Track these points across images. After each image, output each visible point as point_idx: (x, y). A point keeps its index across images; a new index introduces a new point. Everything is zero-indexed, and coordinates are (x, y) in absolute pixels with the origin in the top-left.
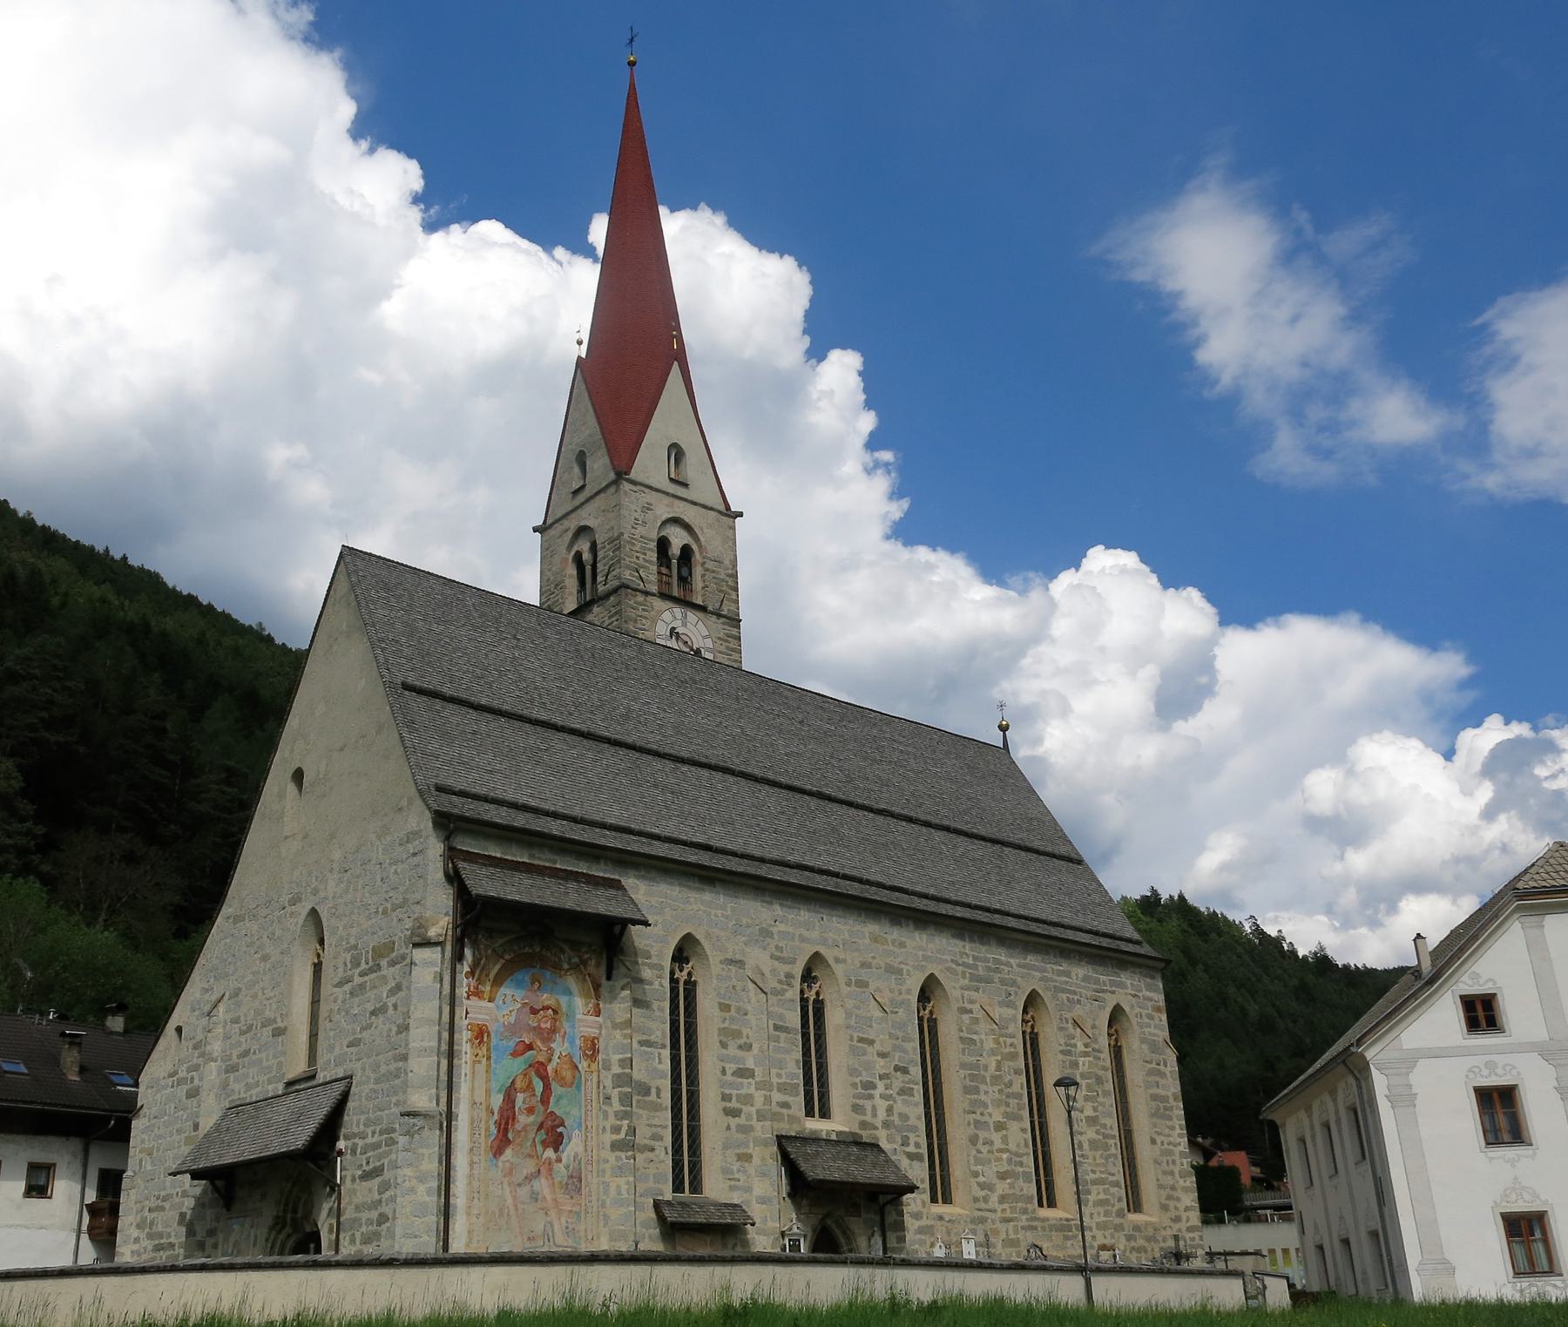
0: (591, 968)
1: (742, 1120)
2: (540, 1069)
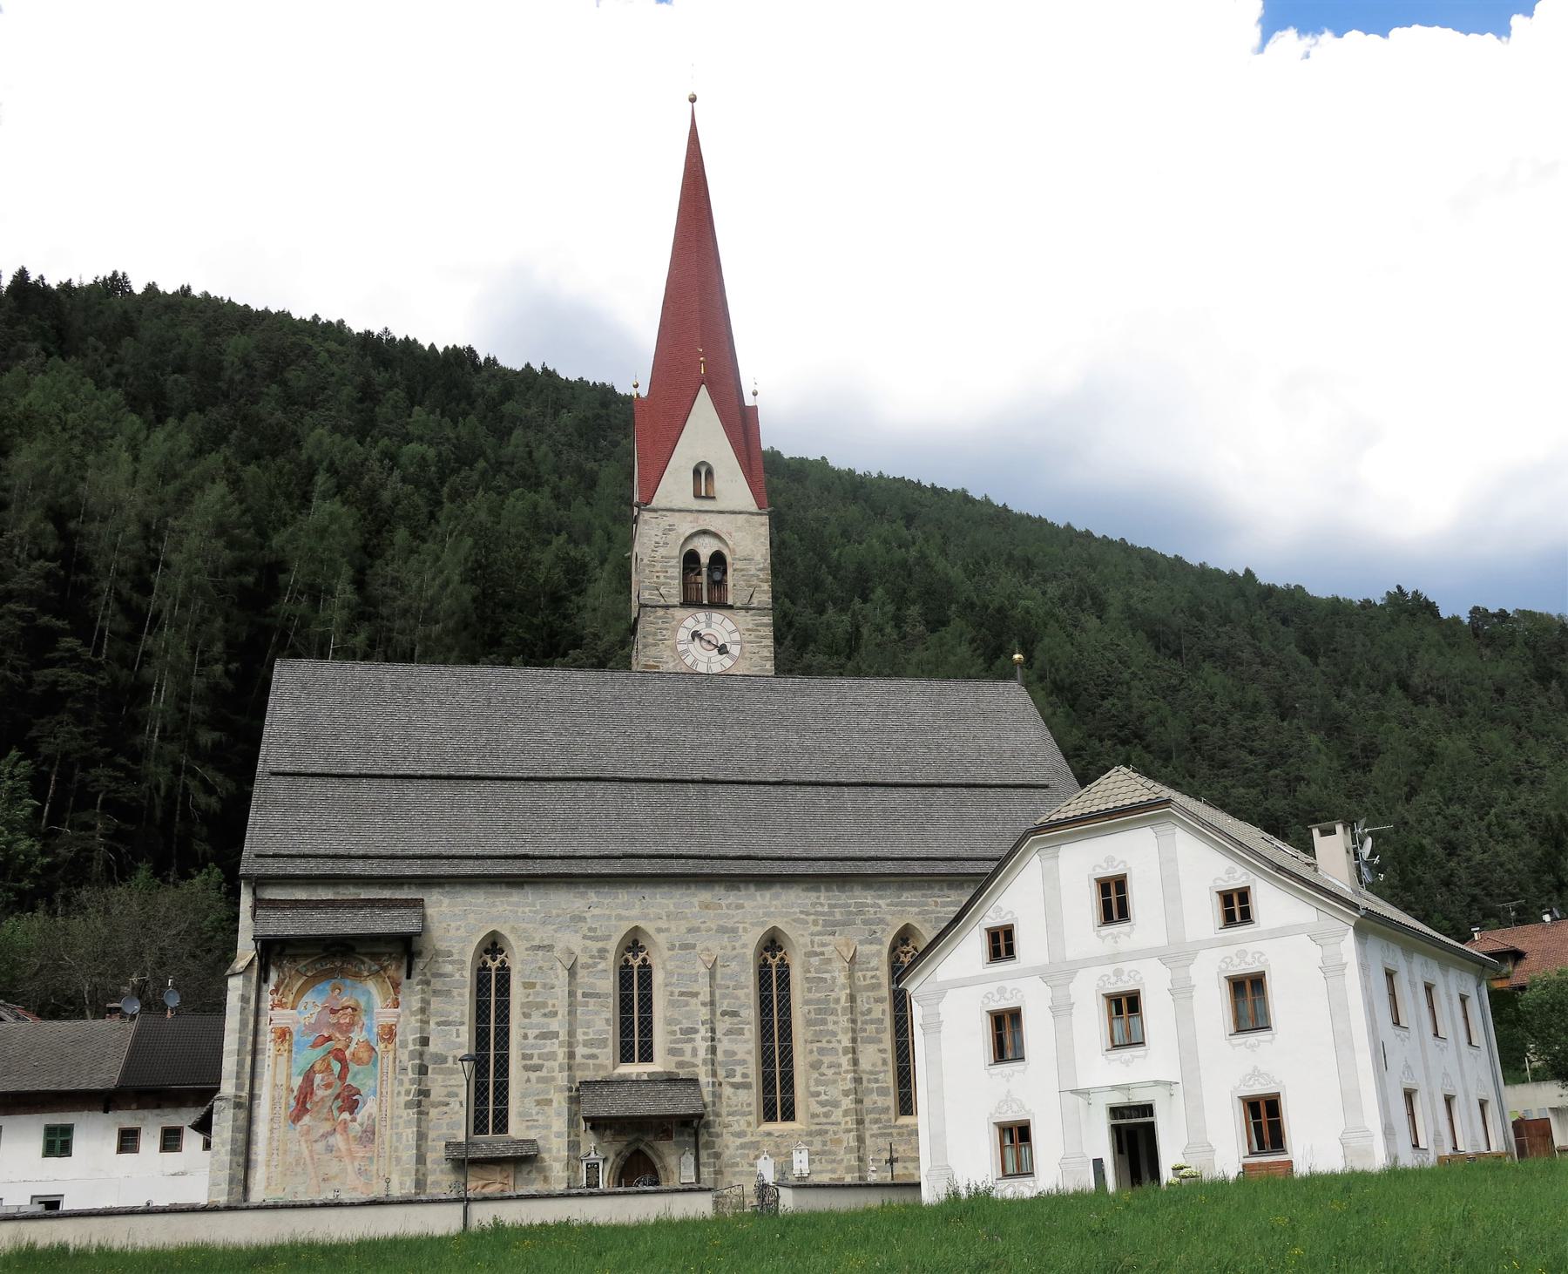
0: (392, 971)
1: (544, 1073)
2: (339, 1055)
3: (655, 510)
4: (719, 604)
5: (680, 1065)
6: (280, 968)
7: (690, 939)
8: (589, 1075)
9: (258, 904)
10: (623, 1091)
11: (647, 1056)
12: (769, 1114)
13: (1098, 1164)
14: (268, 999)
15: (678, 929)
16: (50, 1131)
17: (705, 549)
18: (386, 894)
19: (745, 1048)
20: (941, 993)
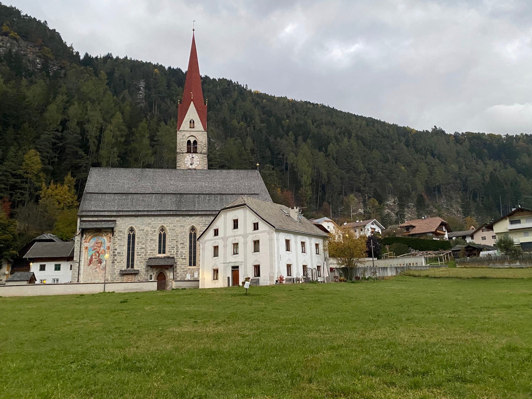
0: (109, 235)
1: (141, 256)
2: (98, 252)
4: (195, 152)
5: (171, 254)
6: (86, 234)
7: (174, 228)
9: (81, 221)
10: (417, 236)
11: (164, 253)
12: (190, 265)
13: (229, 278)
14: (83, 241)
15: (171, 226)
16: (56, 265)
17: (192, 140)
18: (108, 219)
19: (186, 251)
20: (205, 242)
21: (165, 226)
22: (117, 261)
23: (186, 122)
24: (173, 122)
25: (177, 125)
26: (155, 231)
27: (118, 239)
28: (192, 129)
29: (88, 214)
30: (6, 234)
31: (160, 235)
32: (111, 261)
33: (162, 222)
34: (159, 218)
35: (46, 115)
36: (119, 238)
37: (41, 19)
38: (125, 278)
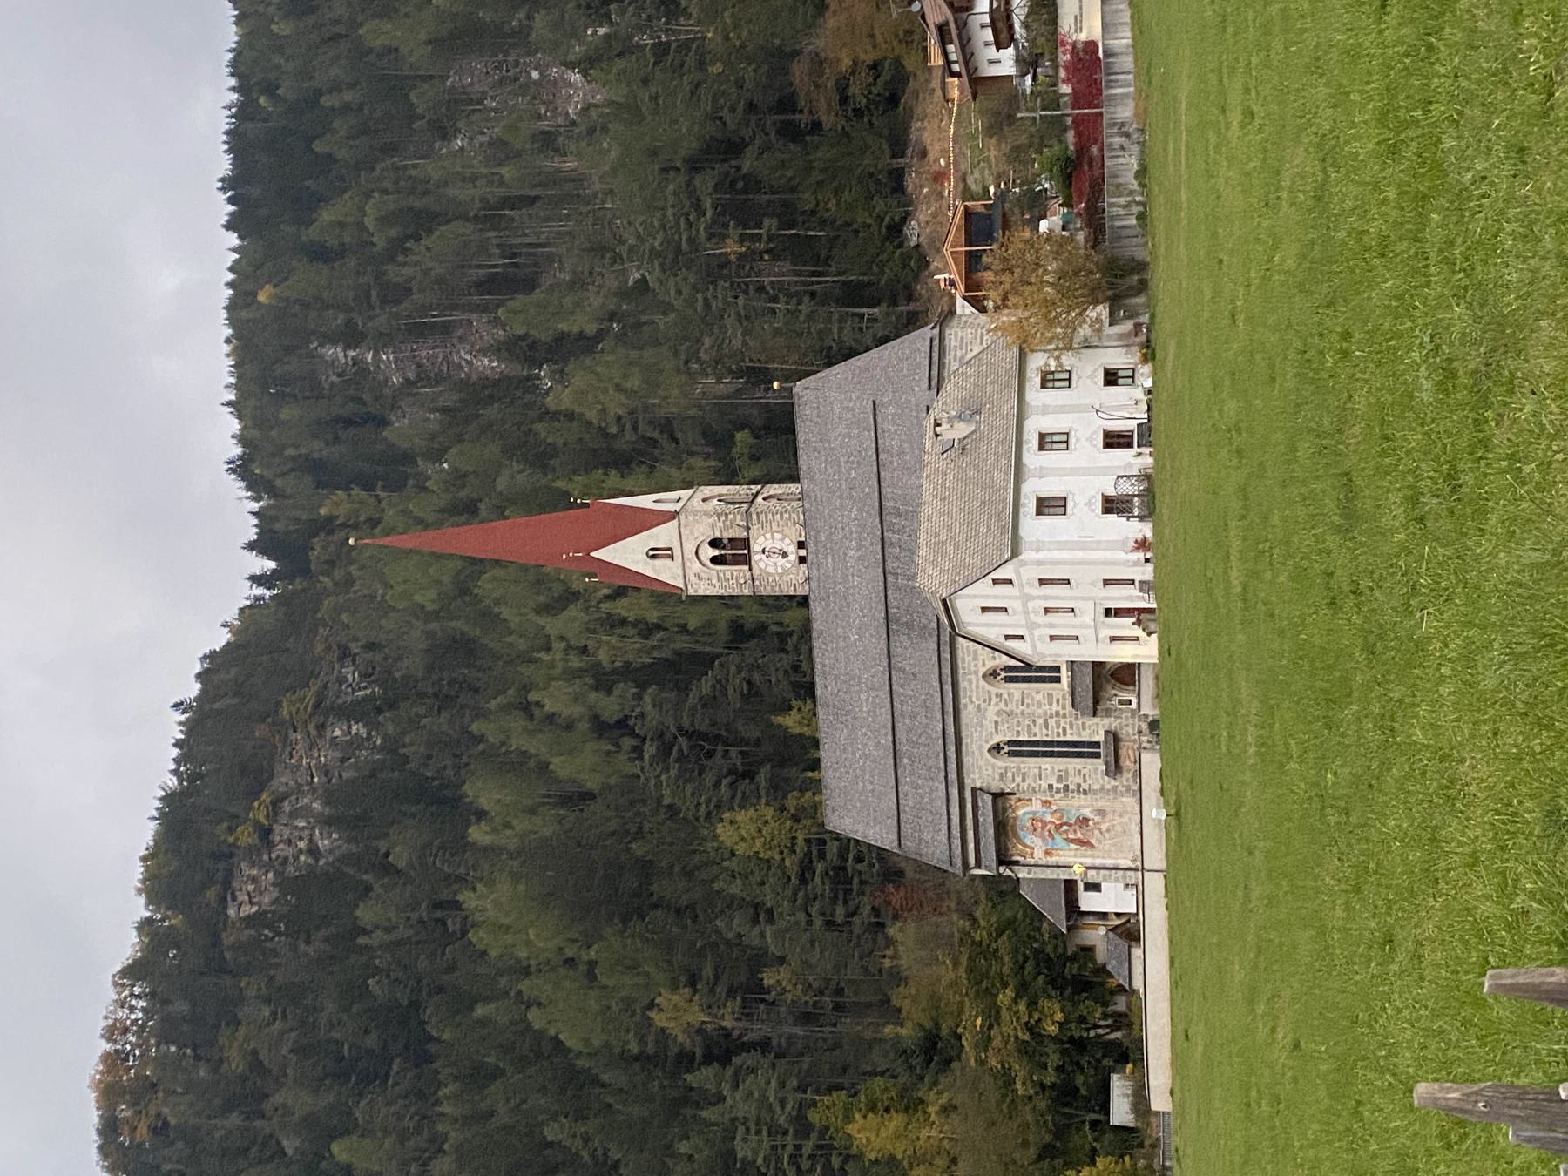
2: (1058, 827)
3: (686, 585)
4: (745, 543)
8: (1069, 702)
9: (978, 865)
14: (1029, 860)
18: (969, 806)
20: (1039, 654)
21: (982, 671)
22: (1081, 781)
23: (656, 572)
24: (515, 313)
25: (666, 595)
26: (999, 695)
27: (1023, 781)
28: (677, 553)
29: (958, 852)
30: (996, 950)
31: (1008, 680)
32: (1082, 796)
33: (973, 677)
34: (963, 684)
35: (592, 783)
36: (1018, 779)
37: (173, 727)
38: (1127, 763)
